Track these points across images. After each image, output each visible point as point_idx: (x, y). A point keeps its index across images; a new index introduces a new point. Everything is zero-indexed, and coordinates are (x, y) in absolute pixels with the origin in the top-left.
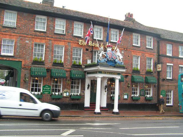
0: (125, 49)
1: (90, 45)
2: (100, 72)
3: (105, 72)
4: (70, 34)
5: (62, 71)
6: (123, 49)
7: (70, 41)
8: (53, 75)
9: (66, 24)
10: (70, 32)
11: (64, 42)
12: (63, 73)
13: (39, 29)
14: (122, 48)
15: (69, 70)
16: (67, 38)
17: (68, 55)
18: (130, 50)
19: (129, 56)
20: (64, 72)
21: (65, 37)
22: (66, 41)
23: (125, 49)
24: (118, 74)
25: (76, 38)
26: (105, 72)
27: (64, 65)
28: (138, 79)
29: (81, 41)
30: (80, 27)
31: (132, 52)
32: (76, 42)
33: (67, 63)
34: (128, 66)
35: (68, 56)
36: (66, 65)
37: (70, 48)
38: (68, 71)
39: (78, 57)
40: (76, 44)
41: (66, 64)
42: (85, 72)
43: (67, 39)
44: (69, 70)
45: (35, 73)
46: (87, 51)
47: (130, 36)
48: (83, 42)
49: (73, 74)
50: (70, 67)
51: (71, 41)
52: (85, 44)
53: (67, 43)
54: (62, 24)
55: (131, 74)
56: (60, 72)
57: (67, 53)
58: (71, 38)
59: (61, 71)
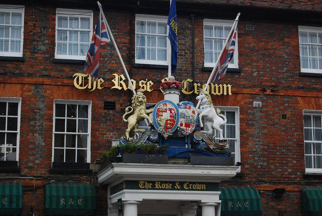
0: (268, 92)
1: (117, 86)
2: (133, 183)
3: (154, 183)
4: (39, 56)
5: (246, 191)
6: (257, 90)
7: (41, 80)
8: (311, 209)
9: (25, 23)
10: (43, 48)
11: (19, 86)
12: (11, 196)
13: (149, 59)
14: (254, 86)
15: (39, 182)
16: (31, 71)
17: (35, 131)
18: (290, 92)
19: (284, 117)
20: (254, 197)
21: (24, 67)
22: (27, 80)
23: (268, 92)
24: (210, 185)
25: (67, 70)
26: (152, 183)
27: (22, 167)
28: (232, 200)
29: (80, 75)
30: (158, 32)
31: (299, 99)
32: (66, 81)
33: (31, 158)
34: (282, 154)
35: (35, 135)
36: (31, 168)
37: (42, 106)
38: (38, 187)
39: (313, 141)
40: (66, 89)
41: (30, 164)
42: (105, 186)
43: (30, 75)
44: (39, 182)
45: (58, 203)
46: (111, 112)
47: (286, 40)
48: (90, 78)
49: (51, 197)
50: (43, 172)
51: (46, 81)
52: (99, 87)
53: (33, 88)
54: (79, 27)
55: (299, 183)
56: (241, 197)
57: (32, 123)
58: (46, 70)
59: (243, 193)
